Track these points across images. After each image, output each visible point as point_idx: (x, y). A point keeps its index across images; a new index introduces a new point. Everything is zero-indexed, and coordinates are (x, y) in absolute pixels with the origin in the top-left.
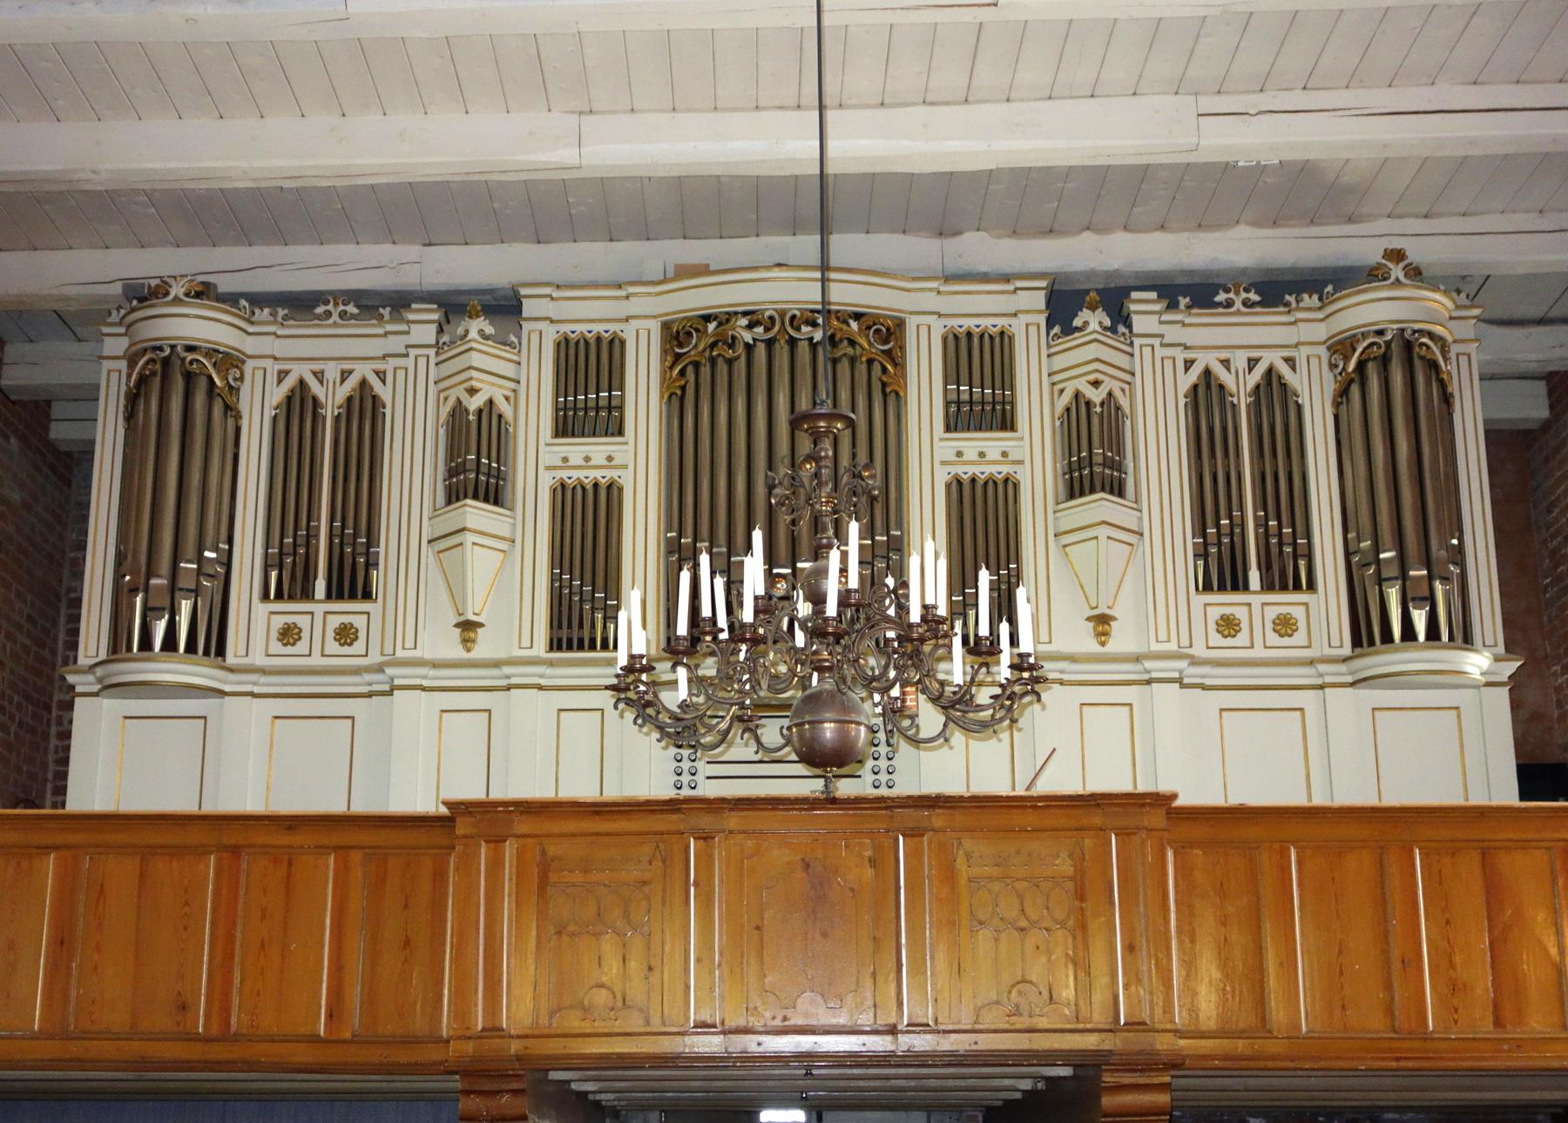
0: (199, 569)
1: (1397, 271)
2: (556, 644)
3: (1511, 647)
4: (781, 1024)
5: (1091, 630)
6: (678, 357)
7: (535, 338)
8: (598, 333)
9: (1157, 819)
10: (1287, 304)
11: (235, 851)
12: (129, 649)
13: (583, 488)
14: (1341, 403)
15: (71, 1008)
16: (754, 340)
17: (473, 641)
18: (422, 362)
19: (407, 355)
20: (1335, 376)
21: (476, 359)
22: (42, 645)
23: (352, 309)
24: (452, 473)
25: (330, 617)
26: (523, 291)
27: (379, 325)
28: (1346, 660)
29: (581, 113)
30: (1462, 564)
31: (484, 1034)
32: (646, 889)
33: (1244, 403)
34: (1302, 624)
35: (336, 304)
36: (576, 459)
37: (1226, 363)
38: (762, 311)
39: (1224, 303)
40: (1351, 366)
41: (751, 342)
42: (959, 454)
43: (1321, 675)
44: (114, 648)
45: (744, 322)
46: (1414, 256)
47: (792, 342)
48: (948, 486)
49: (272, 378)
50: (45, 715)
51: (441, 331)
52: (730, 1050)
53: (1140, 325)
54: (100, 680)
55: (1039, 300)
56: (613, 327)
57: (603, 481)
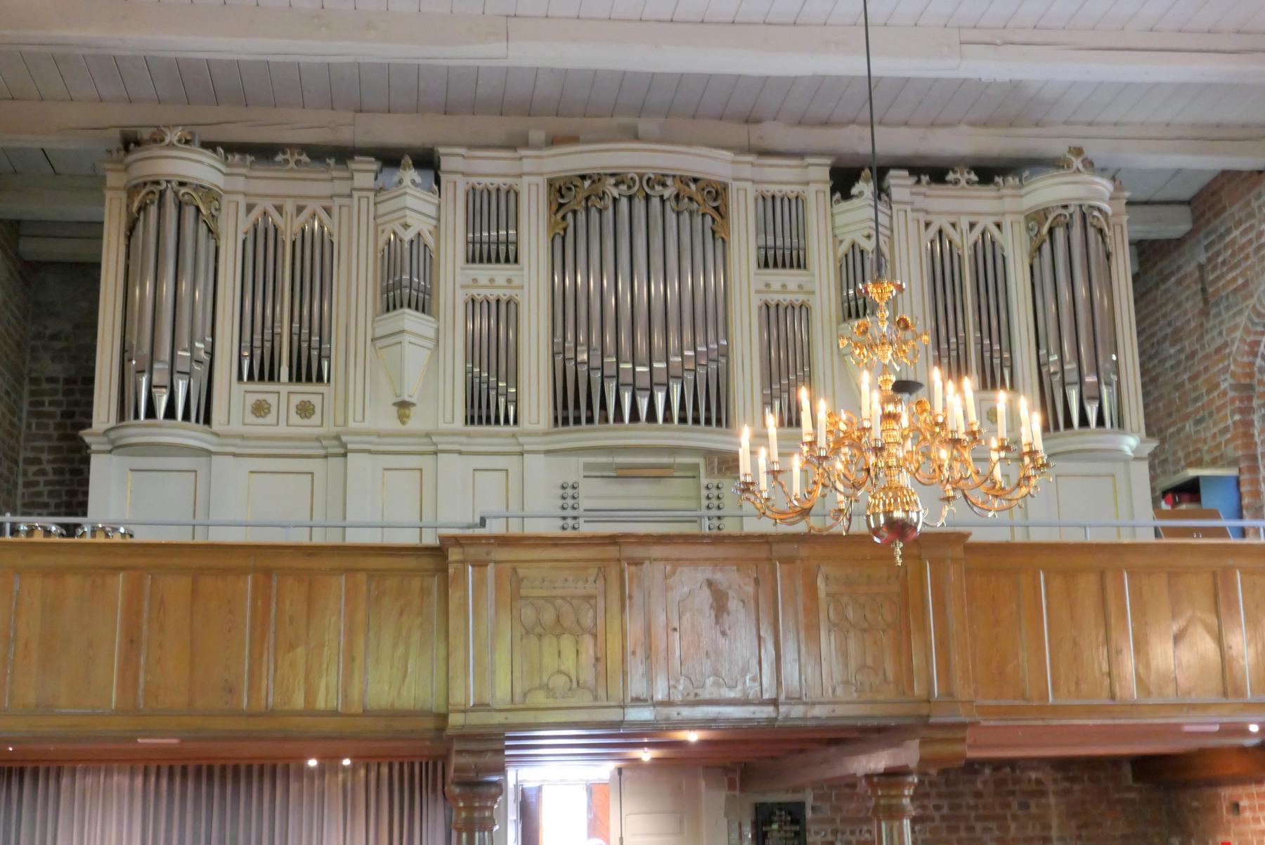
0: (192, 356)
1: (1077, 163)
2: (470, 420)
3: (1150, 433)
4: (693, 699)
5: (396, 411)
6: (561, 206)
7: (451, 187)
8: (499, 185)
9: (958, 551)
10: (997, 184)
11: (268, 573)
12: (137, 416)
13: (488, 302)
14: (1036, 257)
15: (140, 693)
16: (620, 195)
17: (408, 417)
18: (364, 202)
19: (350, 196)
20: (1031, 238)
21: (410, 201)
22: (13, 414)
23: (305, 158)
24: (387, 290)
25: (292, 396)
26: (441, 150)
27: (327, 171)
28: (545, 434)
29: (507, 16)
30: (1118, 373)
31: (475, 708)
32: (593, 602)
33: (967, 254)
34: (318, 409)
35: (292, 155)
36: (483, 280)
37: (279, 209)
38: (626, 174)
39: (953, 181)
40: (1045, 230)
41: (617, 196)
42: (768, 285)
43: (325, 448)
44: (122, 416)
45: (612, 181)
46: (1088, 153)
47: (648, 198)
48: (760, 308)
49: (242, 209)
50: (15, 468)
51: (376, 178)
52: (657, 718)
53: (896, 193)
54: (112, 442)
55: (825, 173)
56: (509, 181)
57: (505, 298)
